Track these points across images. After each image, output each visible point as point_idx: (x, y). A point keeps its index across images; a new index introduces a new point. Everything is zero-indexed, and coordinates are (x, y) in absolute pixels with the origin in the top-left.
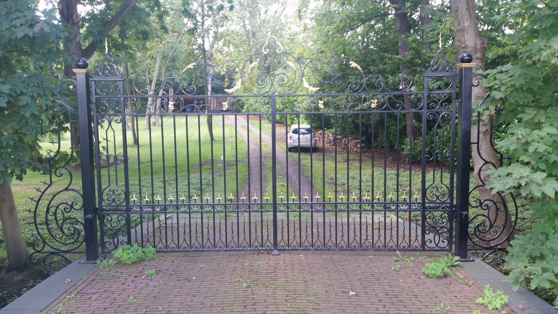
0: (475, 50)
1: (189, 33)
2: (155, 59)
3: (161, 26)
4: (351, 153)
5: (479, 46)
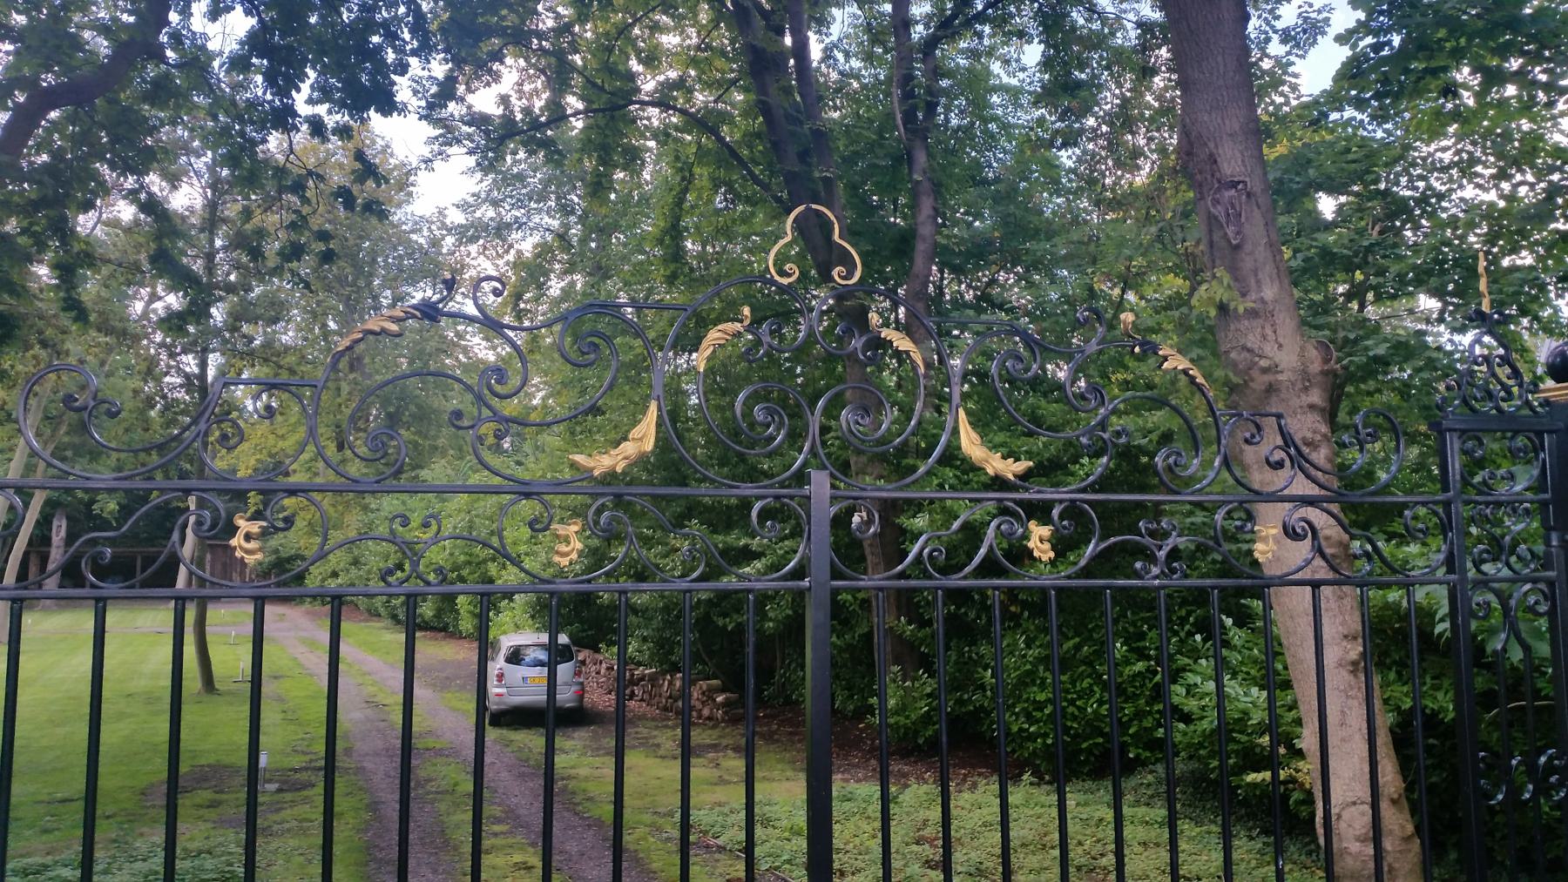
0: (1303, 379)
1: (167, 325)
2: (16, 421)
3: (65, 300)
4: (695, 724)
5: (1316, 367)
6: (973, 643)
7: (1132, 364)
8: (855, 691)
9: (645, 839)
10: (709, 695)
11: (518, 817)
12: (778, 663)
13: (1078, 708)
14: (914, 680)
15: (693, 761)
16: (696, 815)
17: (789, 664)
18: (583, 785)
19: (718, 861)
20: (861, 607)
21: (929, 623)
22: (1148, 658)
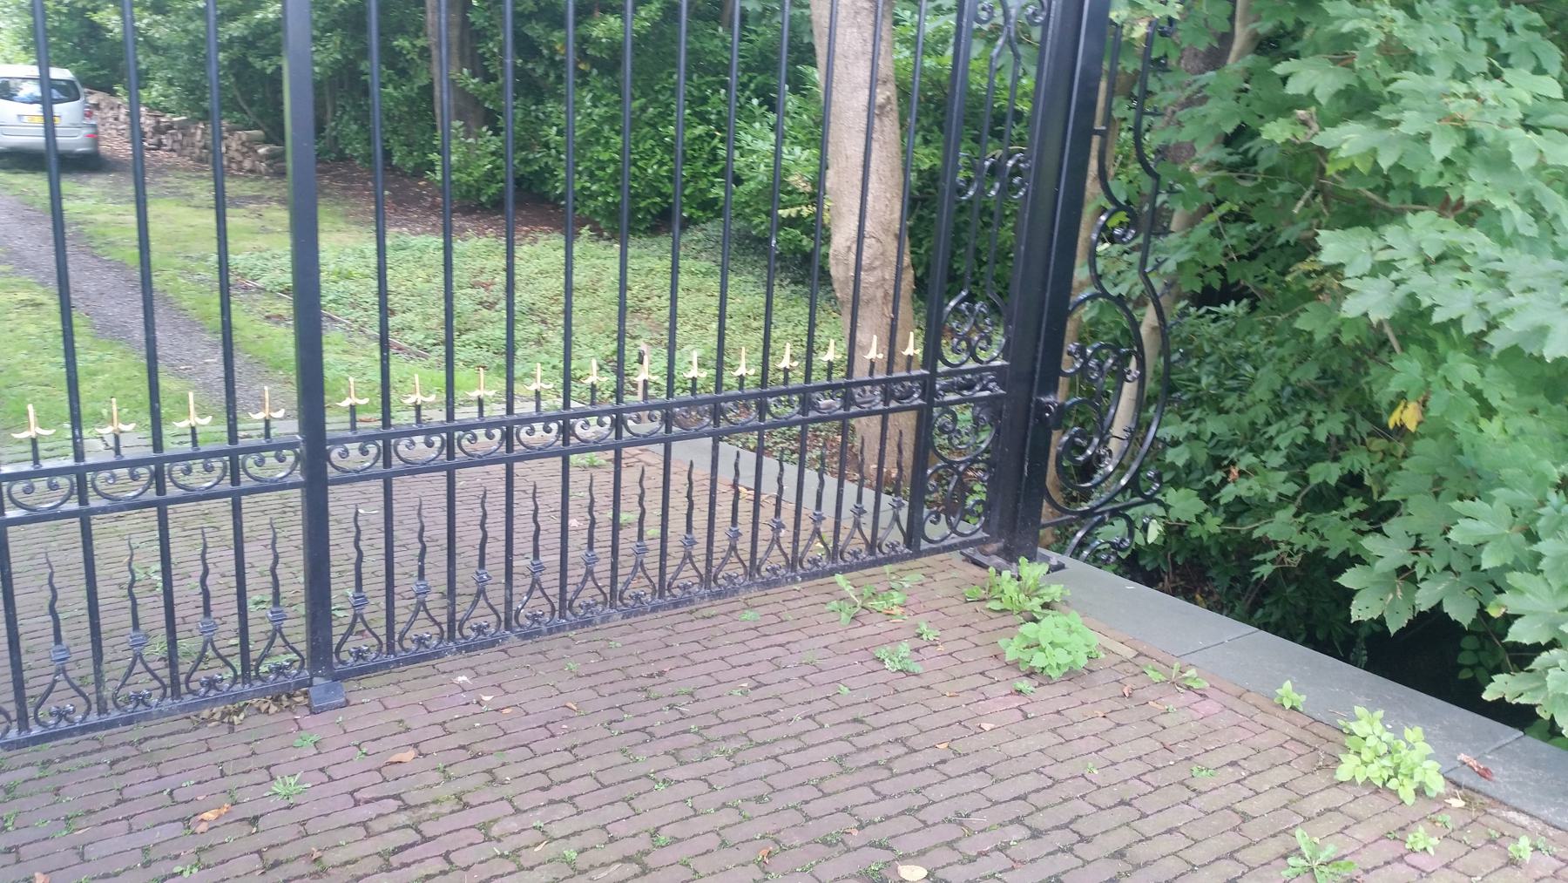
4: (233, 176)
6: (539, 102)
7: (1541, 511)
8: (415, 148)
9: (174, 279)
10: (249, 147)
11: (24, 258)
12: (329, 116)
13: (639, 168)
14: (479, 136)
15: (229, 211)
16: (235, 259)
17: (341, 117)
18: (102, 230)
19: (256, 300)
20: (420, 56)
21: (494, 78)
22: (709, 122)
